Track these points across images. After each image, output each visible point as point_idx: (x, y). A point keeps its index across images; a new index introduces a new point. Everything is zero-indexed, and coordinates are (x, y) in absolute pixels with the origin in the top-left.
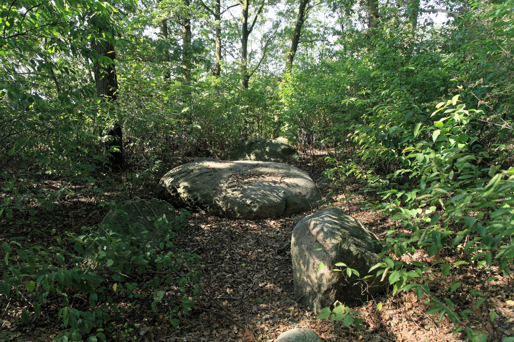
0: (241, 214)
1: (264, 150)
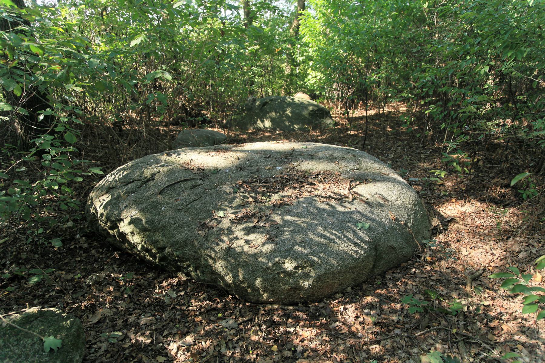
0: (272, 293)
1: (283, 114)
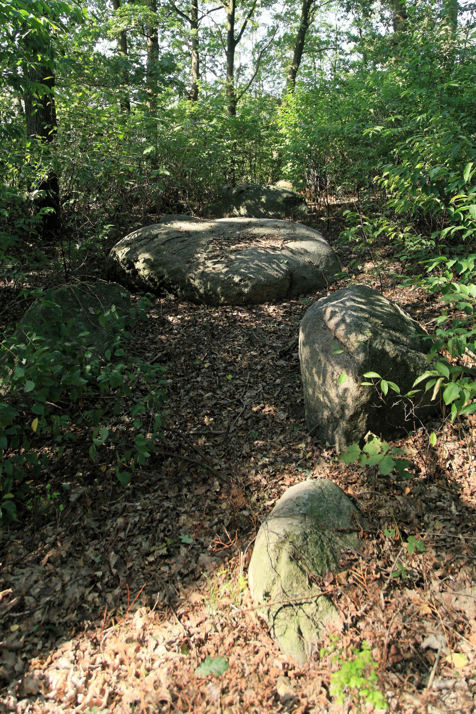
0: (227, 297)
